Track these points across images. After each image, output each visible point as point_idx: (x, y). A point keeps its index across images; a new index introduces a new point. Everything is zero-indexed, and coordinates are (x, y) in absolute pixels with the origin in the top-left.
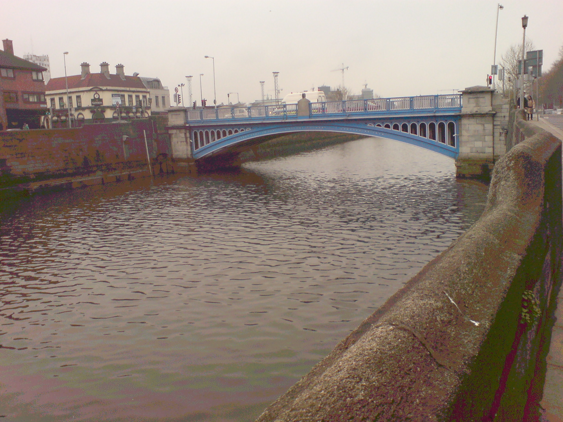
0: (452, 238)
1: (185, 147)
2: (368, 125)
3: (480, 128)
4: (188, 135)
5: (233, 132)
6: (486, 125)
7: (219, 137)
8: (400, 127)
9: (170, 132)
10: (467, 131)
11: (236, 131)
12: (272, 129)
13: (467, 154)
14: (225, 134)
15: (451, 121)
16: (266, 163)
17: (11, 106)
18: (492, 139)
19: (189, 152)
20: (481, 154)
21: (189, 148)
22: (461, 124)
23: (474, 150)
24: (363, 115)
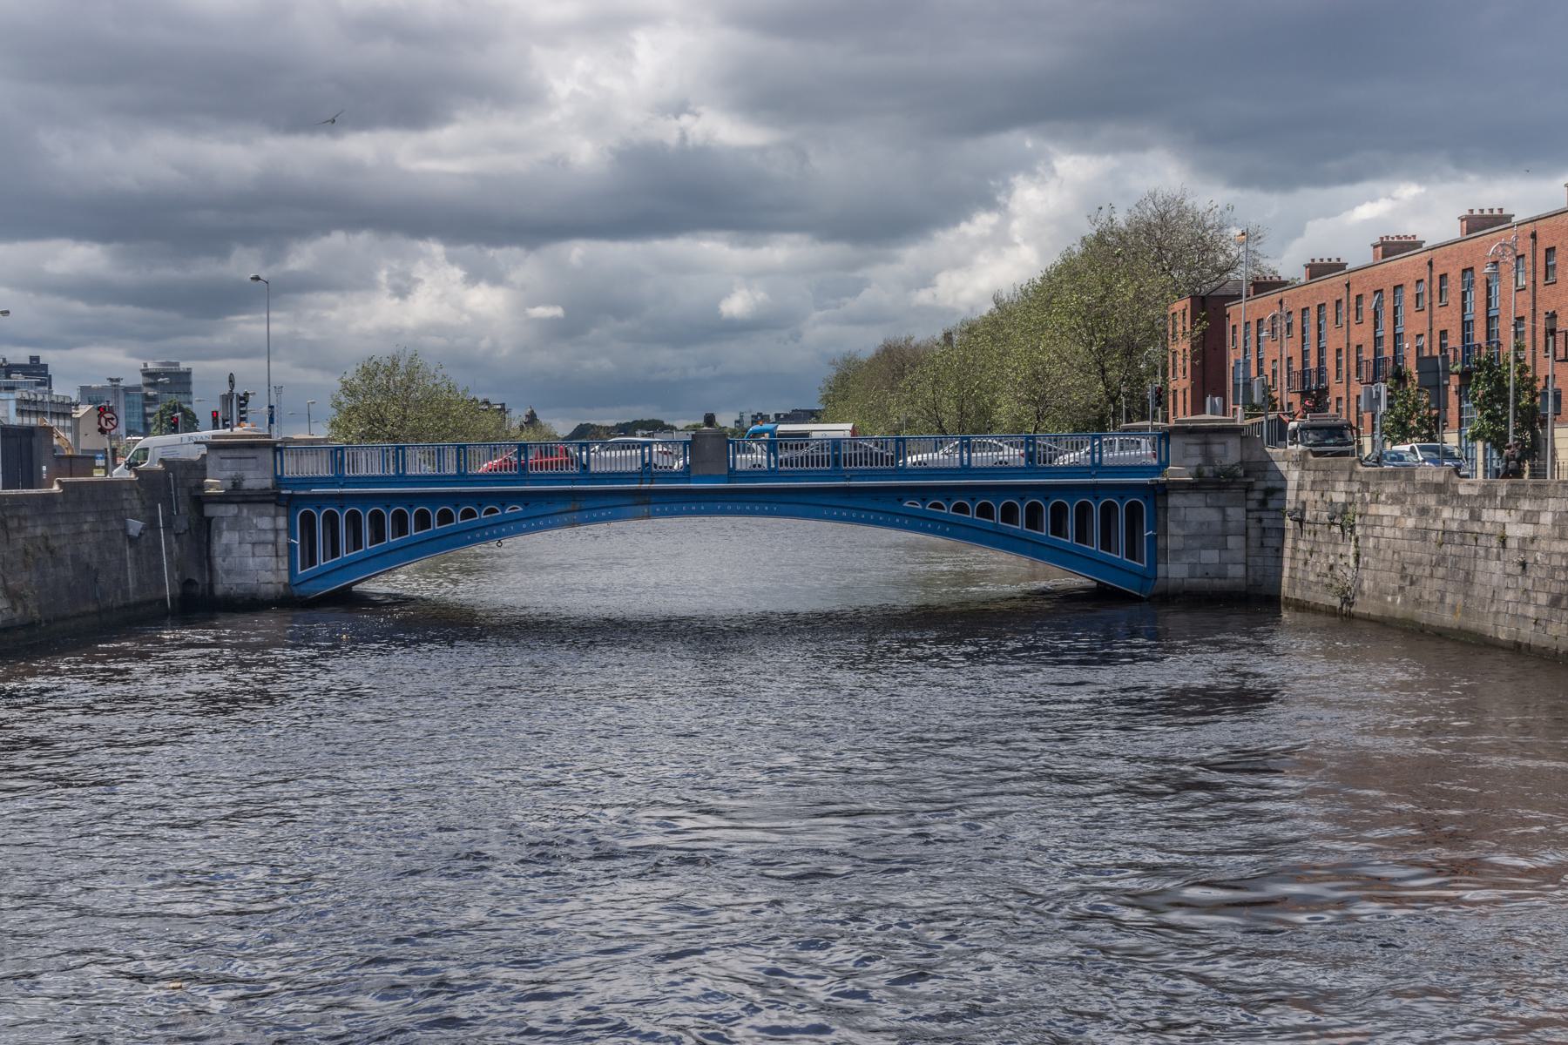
0: (1344, 301)
2: (906, 504)
3: (1213, 515)
4: (282, 522)
5: (434, 518)
6: (1230, 511)
7: (378, 536)
8: (997, 512)
9: (210, 510)
10: (1182, 523)
11: (468, 514)
12: (824, 506)
13: (1180, 581)
19: (285, 576)
23: (1199, 571)
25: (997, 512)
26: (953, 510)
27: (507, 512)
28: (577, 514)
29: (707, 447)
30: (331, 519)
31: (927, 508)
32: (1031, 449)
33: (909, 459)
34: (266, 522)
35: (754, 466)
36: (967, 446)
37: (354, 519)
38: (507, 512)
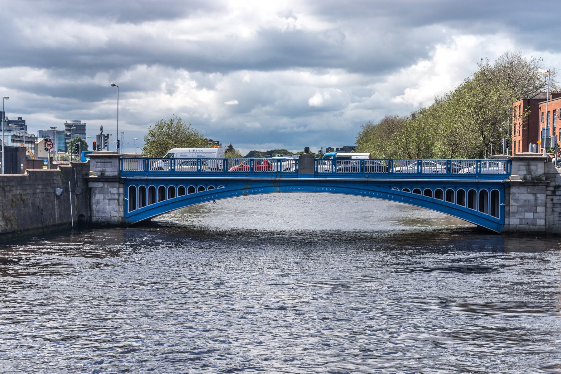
1: (117, 208)
2: (392, 189)
3: (531, 197)
4: (121, 191)
6: (539, 195)
7: (162, 197)
8: (433, 193)
9: (91, 185)
10: (517, 200)
11: (201, 189)
13: (515, 226)
14: (172, 194)
15: (129, 187)
16: (404, 230)
17: (547, 137)
18: (545, 210)
19: (122, 214)
20: (532, 227)
21: (122, 209)
22: (510, 193)
24: (144, 175)
25: (433, 193)
26: (403, 190)
27: (218, 188)
28: (248, 190)
29: (306, 162)
30: (142, 190)
31: (402, 191)
32: (449, 166)
33: (394, 169)
34: (115, 190)
35: (326, 171)
36: (420, 164)
37: (152, 190)
38: (218, 188)
